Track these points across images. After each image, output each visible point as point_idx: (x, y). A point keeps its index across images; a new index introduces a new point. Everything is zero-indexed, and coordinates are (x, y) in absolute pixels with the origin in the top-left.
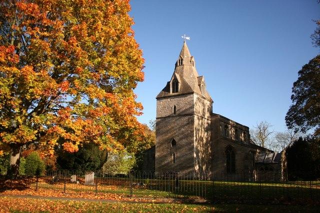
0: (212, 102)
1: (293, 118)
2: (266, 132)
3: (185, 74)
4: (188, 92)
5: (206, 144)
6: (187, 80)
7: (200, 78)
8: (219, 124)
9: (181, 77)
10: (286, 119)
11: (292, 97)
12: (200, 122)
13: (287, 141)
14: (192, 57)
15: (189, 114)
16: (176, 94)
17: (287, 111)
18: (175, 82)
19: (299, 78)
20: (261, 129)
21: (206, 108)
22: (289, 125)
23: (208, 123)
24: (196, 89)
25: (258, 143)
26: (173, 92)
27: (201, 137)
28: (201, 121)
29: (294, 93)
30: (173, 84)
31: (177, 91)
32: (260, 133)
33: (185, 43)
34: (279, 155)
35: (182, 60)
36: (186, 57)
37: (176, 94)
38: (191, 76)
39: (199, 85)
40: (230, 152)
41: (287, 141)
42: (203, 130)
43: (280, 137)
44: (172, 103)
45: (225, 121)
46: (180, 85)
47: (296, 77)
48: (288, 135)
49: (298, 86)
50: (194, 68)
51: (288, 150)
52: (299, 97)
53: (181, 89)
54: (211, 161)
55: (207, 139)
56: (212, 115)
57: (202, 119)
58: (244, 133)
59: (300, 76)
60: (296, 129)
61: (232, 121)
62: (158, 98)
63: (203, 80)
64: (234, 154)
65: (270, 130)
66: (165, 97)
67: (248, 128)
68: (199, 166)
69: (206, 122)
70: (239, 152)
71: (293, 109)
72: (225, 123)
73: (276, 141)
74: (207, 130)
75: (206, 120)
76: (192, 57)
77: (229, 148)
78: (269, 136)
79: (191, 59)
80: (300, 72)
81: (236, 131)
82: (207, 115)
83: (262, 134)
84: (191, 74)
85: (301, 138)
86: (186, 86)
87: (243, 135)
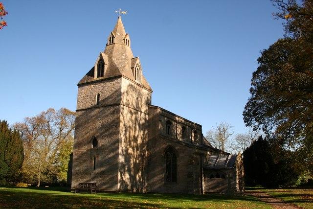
0: (150, 90)
1: (251, 114)
2: (226, 133)
3: (114, 54)
4: (116, 76)
5: (142, 145)
6: (116, 61)
7: (134, 60)
8: (160, 122)
9: (110, 58)
10: (245, 114)
11: (251, 90)
12: (133, 118)
13: (247, 143)
14: (126, 35)
15: (113, 104)
16: (100, 78)
17: (245, 104)
18: (101, 64)
19: (259, 68)
20: (221, 130)
21: (144, 100)
22: (247, 122)
23: (145, 120)
24: (126, 70)
25: (216, 145)
26: (98, 76)
27: (134, 136)
28: (134, 116)
29: (253, 86)
30: (99, 66)
31: (102, 75)
32: (220, 134)
33: (120, 19)
34: (234, 157)
35: (113, 37)
36: (119, 34)
37: (100, 78)
38: (123, 57)
39: (132, 68)
40: (171, 154)
41: (247, 143)
42: (137, 127)
43: (240, 138)
44: (94, 90)
45: (168, 117)
46: (106, 67)
47: (256, 66)
48: (248, 137)
49: (258, 77)
50: (128, 48)
51: (247, 152)
52: (258, 91)
53: (107, 72)
54: (147, 166)
55: (143, 139)
56: (151, 107)
57: (136, 113)
58: (195, 132)
59: (259, 65)
60: (255, 126)
61: (179, 117)
62: (80, 85)
63: (138, 62)
64: (175, 157)
65: (230, 131)
66: (88, 84)
67: (201, 126)
68: (130, 175)
69: (142, 117)
70: (181, 155)
71: (251, 104)
72: (168, 118)
73: (236, 143)
74: (143, 127)
75: (143, 115)
76: (126, 35)
77: (170, 150)
78: (229, 138)
79: (125, 37)
80: (259, 60)
81: (184, 129)
82: (144, 109)
83: (221, 136)
84: (123, 54)
85: (260, 138)
86: (113, 67)
87: (193, 134)
